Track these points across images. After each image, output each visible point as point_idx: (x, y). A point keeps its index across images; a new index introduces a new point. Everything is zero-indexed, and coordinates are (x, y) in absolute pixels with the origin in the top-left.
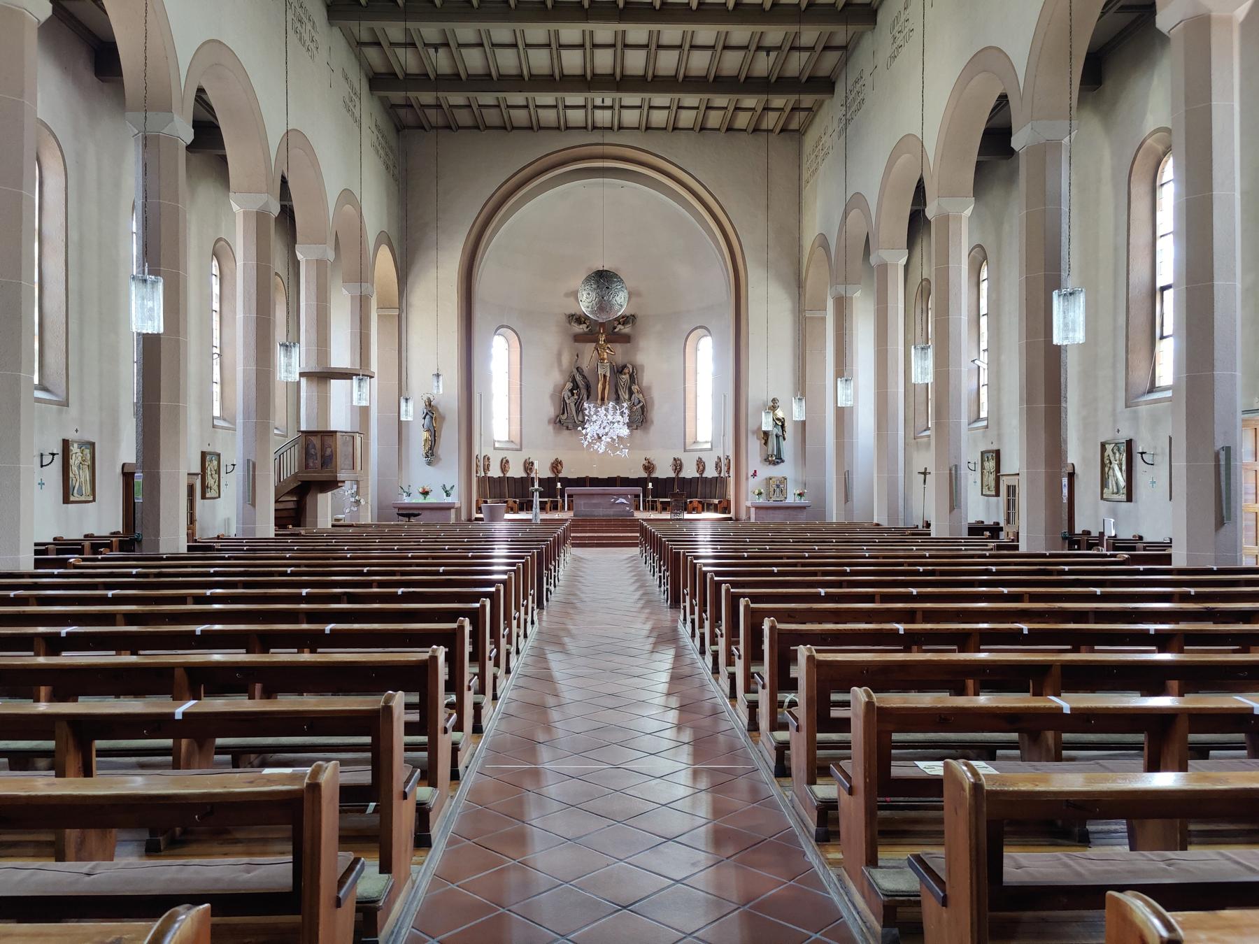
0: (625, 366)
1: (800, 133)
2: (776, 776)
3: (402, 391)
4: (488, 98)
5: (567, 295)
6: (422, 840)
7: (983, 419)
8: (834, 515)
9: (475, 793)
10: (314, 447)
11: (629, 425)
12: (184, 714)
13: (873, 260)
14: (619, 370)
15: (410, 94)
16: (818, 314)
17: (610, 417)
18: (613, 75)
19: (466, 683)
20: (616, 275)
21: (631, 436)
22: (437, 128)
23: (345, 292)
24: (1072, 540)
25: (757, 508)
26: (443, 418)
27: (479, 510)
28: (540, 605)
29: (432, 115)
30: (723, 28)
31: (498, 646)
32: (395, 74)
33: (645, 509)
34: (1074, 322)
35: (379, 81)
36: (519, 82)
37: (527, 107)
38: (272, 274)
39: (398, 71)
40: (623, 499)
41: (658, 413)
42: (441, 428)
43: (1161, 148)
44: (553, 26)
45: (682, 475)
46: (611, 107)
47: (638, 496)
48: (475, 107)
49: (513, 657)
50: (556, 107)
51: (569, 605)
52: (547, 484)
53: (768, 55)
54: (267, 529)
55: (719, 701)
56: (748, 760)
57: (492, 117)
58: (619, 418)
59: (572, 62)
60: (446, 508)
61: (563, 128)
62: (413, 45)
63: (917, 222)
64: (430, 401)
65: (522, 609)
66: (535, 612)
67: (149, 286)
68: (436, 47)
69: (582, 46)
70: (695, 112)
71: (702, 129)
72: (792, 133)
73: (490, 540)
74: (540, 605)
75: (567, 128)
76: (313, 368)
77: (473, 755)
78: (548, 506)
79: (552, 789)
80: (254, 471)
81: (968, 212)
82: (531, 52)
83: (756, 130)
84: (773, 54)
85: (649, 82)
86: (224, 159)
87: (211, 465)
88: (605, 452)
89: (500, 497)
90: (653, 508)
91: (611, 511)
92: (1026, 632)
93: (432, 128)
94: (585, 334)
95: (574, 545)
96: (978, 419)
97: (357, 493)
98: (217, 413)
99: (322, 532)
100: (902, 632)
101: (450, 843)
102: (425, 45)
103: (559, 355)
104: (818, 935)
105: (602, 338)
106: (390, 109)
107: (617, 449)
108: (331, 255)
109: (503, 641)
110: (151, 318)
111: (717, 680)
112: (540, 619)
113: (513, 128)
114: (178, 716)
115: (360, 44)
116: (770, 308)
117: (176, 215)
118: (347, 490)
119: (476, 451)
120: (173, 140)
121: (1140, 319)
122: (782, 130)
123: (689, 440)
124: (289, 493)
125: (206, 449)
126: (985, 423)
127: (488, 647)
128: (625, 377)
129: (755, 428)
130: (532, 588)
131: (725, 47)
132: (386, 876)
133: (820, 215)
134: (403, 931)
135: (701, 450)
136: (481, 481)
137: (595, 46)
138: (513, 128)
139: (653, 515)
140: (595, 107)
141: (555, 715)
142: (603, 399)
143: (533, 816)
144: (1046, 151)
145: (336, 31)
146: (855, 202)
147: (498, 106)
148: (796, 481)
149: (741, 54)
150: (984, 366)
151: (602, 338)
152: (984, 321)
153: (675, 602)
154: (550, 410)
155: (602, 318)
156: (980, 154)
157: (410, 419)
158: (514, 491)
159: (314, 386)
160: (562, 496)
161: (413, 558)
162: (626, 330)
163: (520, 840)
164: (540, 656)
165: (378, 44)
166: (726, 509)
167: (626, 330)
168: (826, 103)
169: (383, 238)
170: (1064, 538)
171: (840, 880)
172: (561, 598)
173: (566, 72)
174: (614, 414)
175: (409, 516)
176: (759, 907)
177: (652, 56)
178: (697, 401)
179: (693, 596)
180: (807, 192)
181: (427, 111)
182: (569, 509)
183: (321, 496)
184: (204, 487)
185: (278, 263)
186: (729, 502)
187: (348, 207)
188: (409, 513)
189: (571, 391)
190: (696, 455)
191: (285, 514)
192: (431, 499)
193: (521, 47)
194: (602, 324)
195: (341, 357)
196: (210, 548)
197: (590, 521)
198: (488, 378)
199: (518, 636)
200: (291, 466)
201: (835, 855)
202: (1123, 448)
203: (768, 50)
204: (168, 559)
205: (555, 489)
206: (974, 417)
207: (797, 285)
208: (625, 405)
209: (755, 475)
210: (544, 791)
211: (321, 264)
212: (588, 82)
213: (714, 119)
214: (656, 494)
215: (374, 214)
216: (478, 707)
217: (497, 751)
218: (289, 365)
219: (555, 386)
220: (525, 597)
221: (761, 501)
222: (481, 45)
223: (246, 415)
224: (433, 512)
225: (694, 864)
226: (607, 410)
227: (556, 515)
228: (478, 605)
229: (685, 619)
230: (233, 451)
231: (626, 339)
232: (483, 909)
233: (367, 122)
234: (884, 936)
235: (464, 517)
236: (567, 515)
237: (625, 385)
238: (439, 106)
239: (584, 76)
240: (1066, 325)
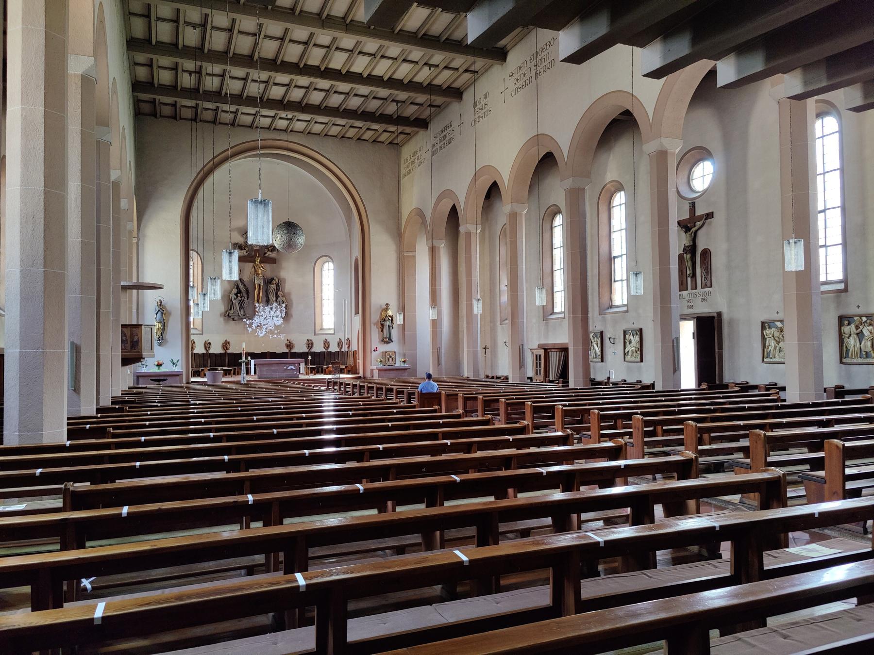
0: (273, 279)
14: (269, 281)
24: (594, 382)
41: (295, 311)
42: (168, 320)
43: (613, 189)
48: (178, 106)
58: (278, 313)
64: (161, 302)
72: (395, 146)
105: (258, 260)
115: (136, 64)
121: (604, 271)
123: (318, 328)
128: (273, 286)
148: (399, 354)
151: (258, 260)
154: (222, 308)
180: (404, 181)
189: (236, 295)
190: (323, 338)
192: (163, 369)
202: (599, 335)
207: (398, 235)
221: (381, 366)
226: (271, 309)
231: (273, 261)
237: (273, 291)
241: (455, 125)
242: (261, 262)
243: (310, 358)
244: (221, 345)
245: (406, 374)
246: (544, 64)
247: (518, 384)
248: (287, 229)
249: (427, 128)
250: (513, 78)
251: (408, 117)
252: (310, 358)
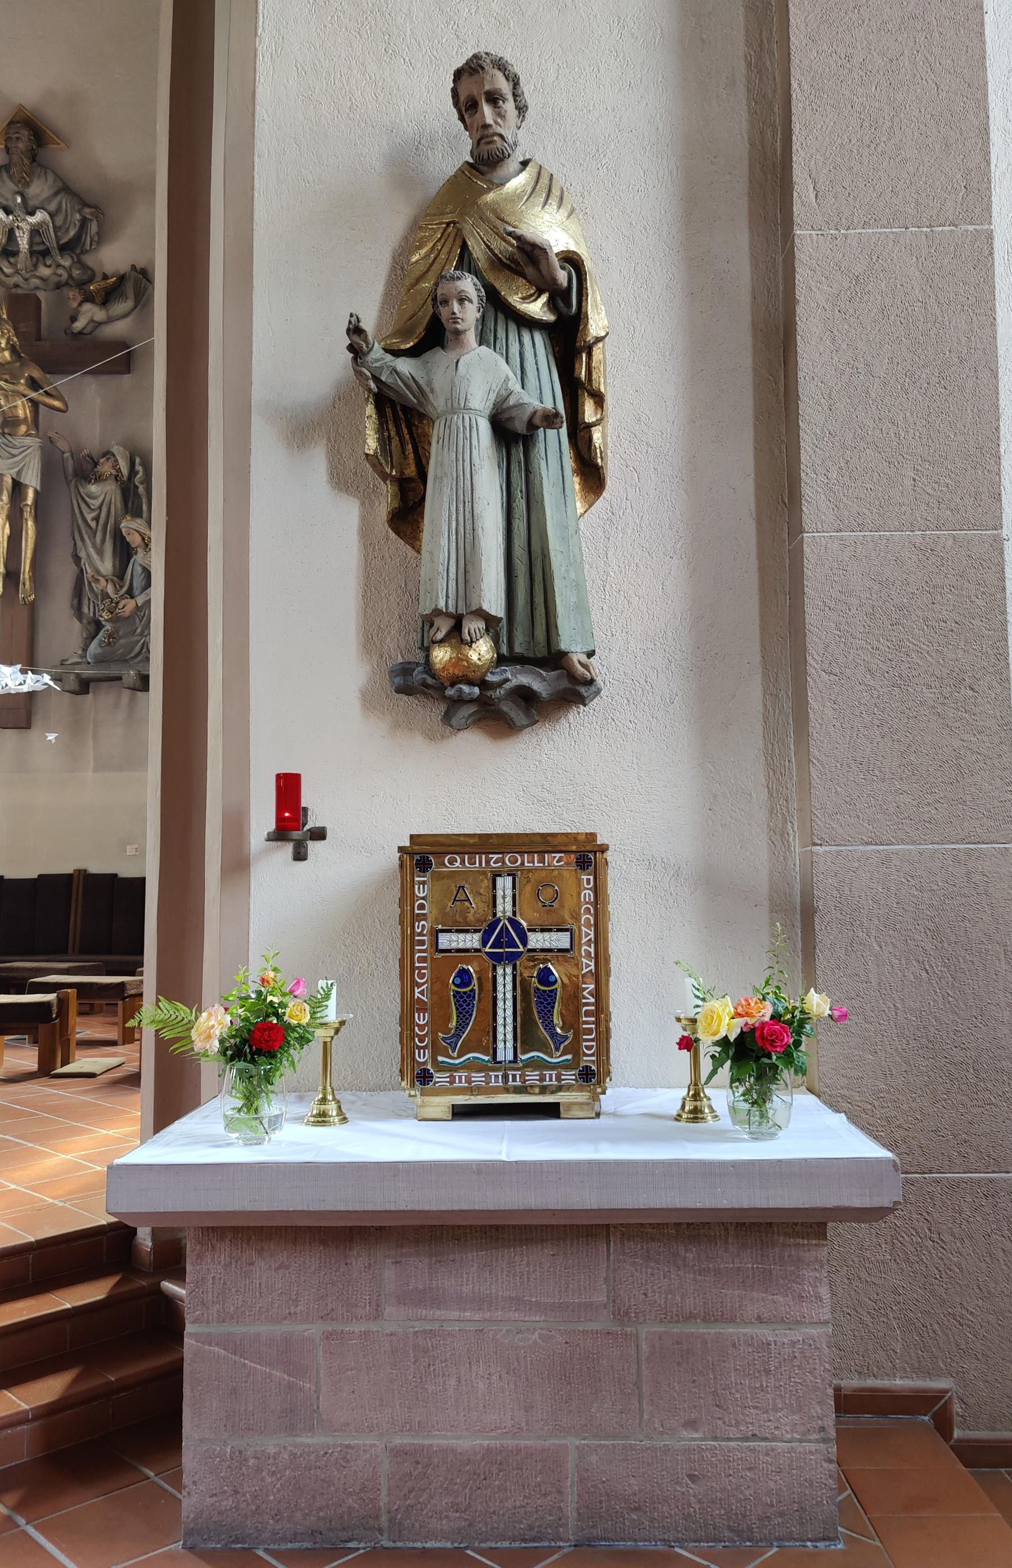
148: (714, 888)
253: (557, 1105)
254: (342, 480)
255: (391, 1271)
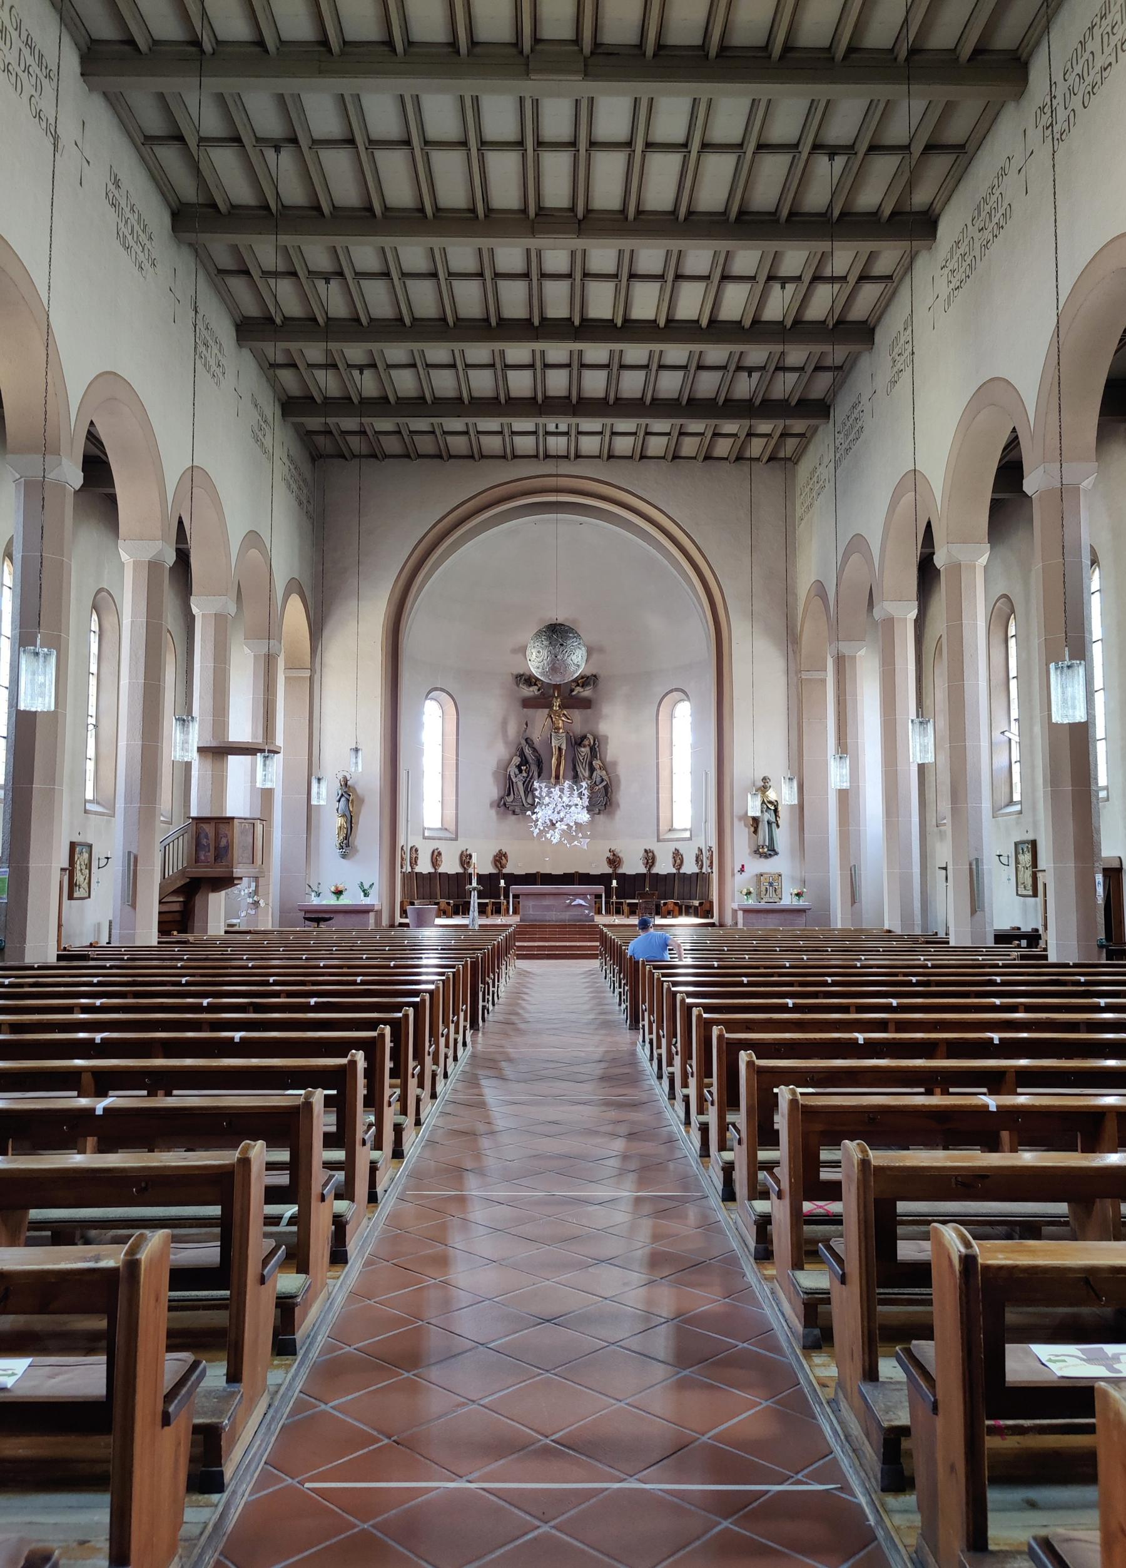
0: (584, 737)
1: (793, 461)
2: (724, 1200)
3: (313, 773)
4: (421, 424)
5: (515, 651)
6: (339, 1257)
7: (1016, 803)
8: (839, 920)
9: (394, 1218)
10: (207, 837)
11: (589, 809)
12: (105, 1109)
13: (877, 613)
14: (577, 742)
15: (330, 420)
16: (817, 675)
17: (565, 799)
18: (568, 398)
19: (386, 1099)
20: (571, 630)
21: (592, 821)
22: (360, 456)
23: (247, 650)
25: (746, 911)
26: (361, 801)
27: (404, 913)
28: (474, 1025)
29: (355, 442)
30: (696, 347)
31: (422, 1064)
32: (312, 398)
33: (608, 912)
34: (1074, 698)
35: (292, 406)
36: (457, 405)
37: (467, 433)
38: (164, 631)
39: (315, 395)
40: (580, 900)
41: (626, 794)
44: (498, 346)
45: (655, 870)
46: (567, 434)
47: (600, 896)
48: (405, 433)
49: (440, 1078)
50: (501, 433)
51: (510, 1026)
52: (489, 883)
53: (750, 376)
54: (148, 935)
55: (675, 1129)
56: (699, 1187)
57: (425, 445)
58: (577, 800)
59: (520, 384)
60: (364, 911)
61: (510, 456)
62: (334, 366)
63: (927, 572)
64: (346, 781)
65: (452, 1026)
66: (468, 1033)
67: (41, 659)
68: (361, 368)
69: (532, 366)
70: (666, 438)
71: (675, 457)
72: (783, 461)
73: (416, 948)
74: (474, 1025)
75: (515, 457)
76: (209, 742)
77: (392, 1180)
78: (489, 908)
79: (478, 1214)
80: (136, 865)
81: (983, 560)
82: (472, 373)
83: (739, 458)
84: (756, 376)
85: (611, 406)
86: (112, 499)
87: (82, 859)
88: (560, 841)
89: (430, 897)
90: (618, 912)
91: (566, 916)
92: (996, 1042)
93: (355, 456)
94: (535, 698)
95: (519, 957)
96: (1011, 802)
97: (256, 892)
98: (89, 795)
99: (212, 942)
100: (861, 1042)
101: (368, 1263)
102: (349, 366)
103: (504, 723)
104: (745, 1345)
105: (557, 703)
106: (306, 437)
107: (575, 838)
108: (232, 609)
109: (428, 1060)
110: (42, 695)
111: (673, 1105)
112: (474, 1042)
113: (451, 457)
114: (99, 1112)
115: (273, 366)
116: (759, 669)
117: (61, 569)
118: (244, 889)
119: (401, 841)
120: (60, 486)
122: (770, 459)
123: (664, 827)
124: (176, 892)
125: (77, 839)
126: (1018, 808)
127: (411, 1063)
128: (585, 750)
129: (742, 813)
130: (465, 1002)
131: (700, 367)
132: (304, 1276)
133: (814, 563)
134: (319, 1338)
135: (678, 840)
136: (407, 877)
137: (546, 366)
138: (451, 457)
139: (617, 920)
140: (547, 433)
141: (485, 1143)
142: (557, 777)
143: (457, 1241)
144: (1064, 495)
145: (246, 353)
146: (858, 544)
147: (433, 432)
148: (793, 878)
149: (718, 375)
150: (1015, 739)
151: (557, 703)
152: (1013, 684)
153: (635, 1022)
154: (493, 791)
155: (557, 680)
156: (995, 490)
157: (322, 803)
158: (446, 891)
159: (209, 763)
160: (507, 897)
161: (325, 967)
162: (587, 693)
163: (442, 1262)
164: (472, 1081)
165: (294, 366)
166: (708, 913)
167: (587, 693)
168: (821, 429)
169: (294, 586)
170: (1101, 947)
171: (772, 1293)
172: (501, 1018)
173: (513, 394)
174: (571, 795)
175: (318, 921)
176: (685, 1321)
177: (614, 377)
178: (672, 781)
179: (651, 1013)
180: (801, 530)
181: (348, 438)
182: (515, 912)
183: (212, 896)
184: (72, 885)
185: (171, 620)
186: (711, 903)
187: (254, 552)
188: (318, 917)
189: (519, 767)
190: (672, 846)
191: (168, 918)
192: (345, 901)
193: (460, 368)
194: (557, 687)
195: (241, 730)
196: (85, 957)
197: (540, 926)
198: (418, 752)
199: (446, 1057)
200: (178, 861)
201: (771, 1271)
203: (750, 370)
204: (39, 968)
205: (497, 888)
206: (1004, 800)
207: (790, 639)
208: (584, 784)
209: (742, 870)
210: (471, 1217)
211: (221, 622)
212: (539, 405)
213: (689, 446)
214: (622, 893)
215: (284, 557)
216: (398, 1129)
217: (418, 1177)
218: (185, 742)
219: (499, 762)
220: (456, 1012)
221: (751, 902)
222: (414, 366)
223: (128, 800)
224: (348, 916)
225: (625, 1284)
226: (562, 790)
227: (499, 920)
228: (400, 1015)
229: (644, 1041)
230: (110, 841)
231: (586, 704)
232: (400, 1322)
233: (279, 453)
234: (805, 1336)
235: (385, 922)
236: (513, 920)
238: (363, 433)
239: (534, 398)
240: (1065, 701)
241: (864, 399)
242: (562, 707)
243: (614, 883)
244: (491, 858)
245: (801, 920)
246: (995, 220)
247: (965, 950)
248: (549, 638)
249: (828, 417)
250: (946, 271)
251: (782, 402)
252: (614, 883)
253: (1079, 650)
254: (746, 825)
255: (762, 915)
